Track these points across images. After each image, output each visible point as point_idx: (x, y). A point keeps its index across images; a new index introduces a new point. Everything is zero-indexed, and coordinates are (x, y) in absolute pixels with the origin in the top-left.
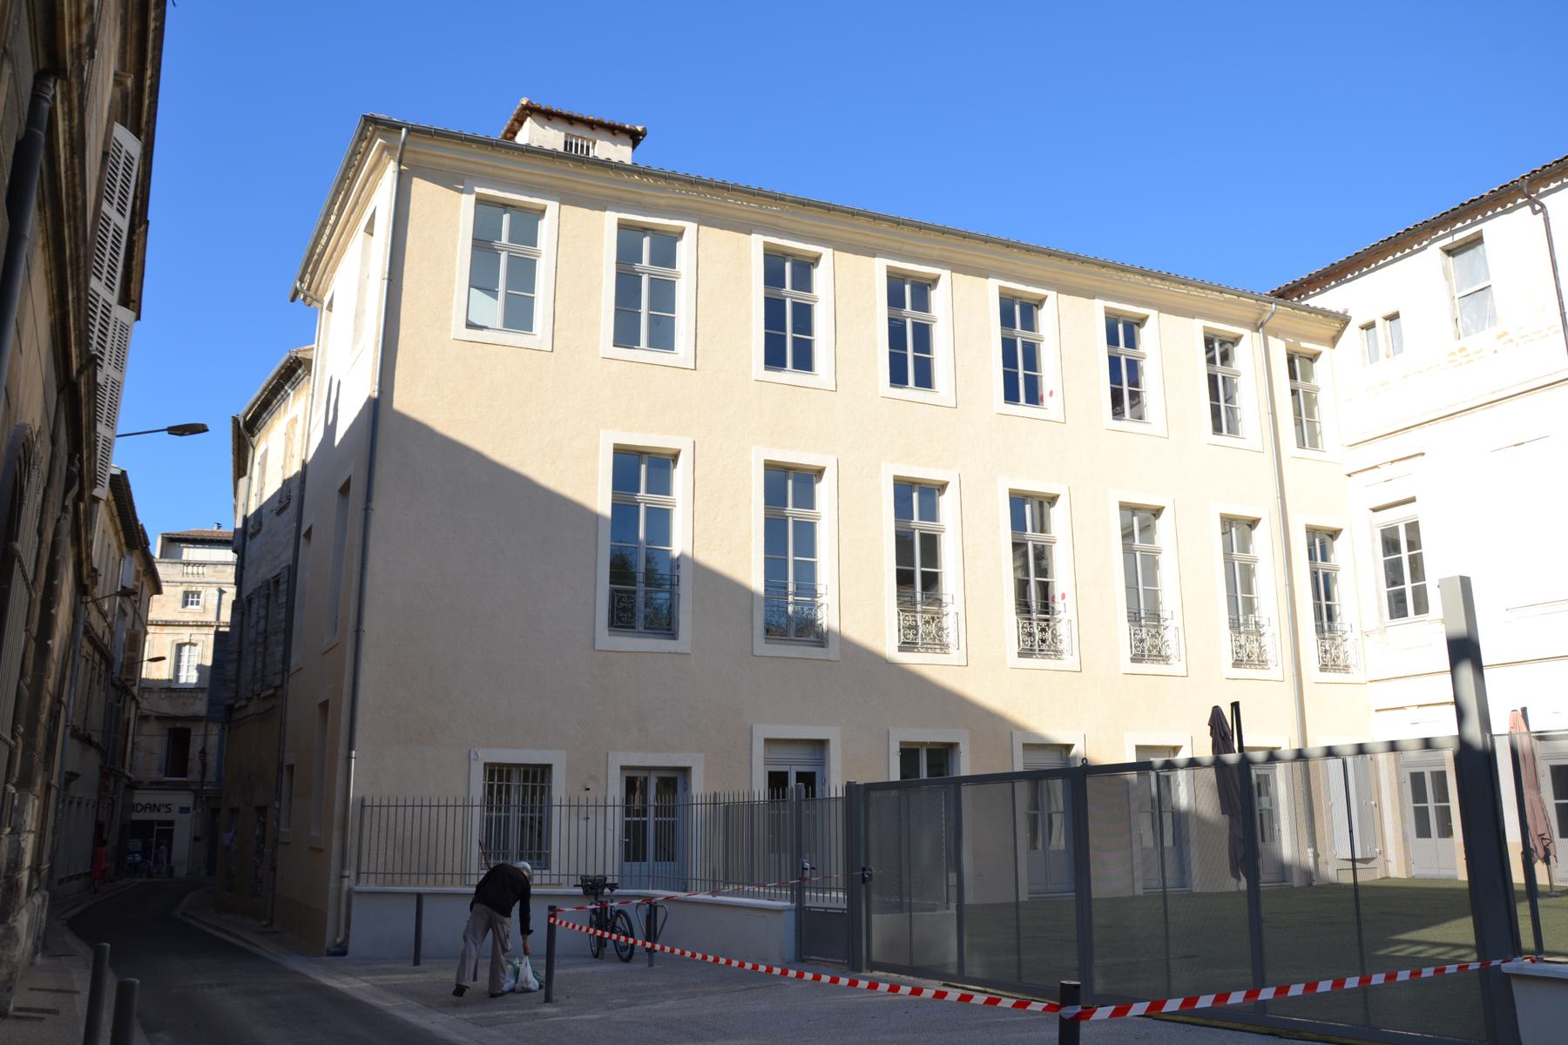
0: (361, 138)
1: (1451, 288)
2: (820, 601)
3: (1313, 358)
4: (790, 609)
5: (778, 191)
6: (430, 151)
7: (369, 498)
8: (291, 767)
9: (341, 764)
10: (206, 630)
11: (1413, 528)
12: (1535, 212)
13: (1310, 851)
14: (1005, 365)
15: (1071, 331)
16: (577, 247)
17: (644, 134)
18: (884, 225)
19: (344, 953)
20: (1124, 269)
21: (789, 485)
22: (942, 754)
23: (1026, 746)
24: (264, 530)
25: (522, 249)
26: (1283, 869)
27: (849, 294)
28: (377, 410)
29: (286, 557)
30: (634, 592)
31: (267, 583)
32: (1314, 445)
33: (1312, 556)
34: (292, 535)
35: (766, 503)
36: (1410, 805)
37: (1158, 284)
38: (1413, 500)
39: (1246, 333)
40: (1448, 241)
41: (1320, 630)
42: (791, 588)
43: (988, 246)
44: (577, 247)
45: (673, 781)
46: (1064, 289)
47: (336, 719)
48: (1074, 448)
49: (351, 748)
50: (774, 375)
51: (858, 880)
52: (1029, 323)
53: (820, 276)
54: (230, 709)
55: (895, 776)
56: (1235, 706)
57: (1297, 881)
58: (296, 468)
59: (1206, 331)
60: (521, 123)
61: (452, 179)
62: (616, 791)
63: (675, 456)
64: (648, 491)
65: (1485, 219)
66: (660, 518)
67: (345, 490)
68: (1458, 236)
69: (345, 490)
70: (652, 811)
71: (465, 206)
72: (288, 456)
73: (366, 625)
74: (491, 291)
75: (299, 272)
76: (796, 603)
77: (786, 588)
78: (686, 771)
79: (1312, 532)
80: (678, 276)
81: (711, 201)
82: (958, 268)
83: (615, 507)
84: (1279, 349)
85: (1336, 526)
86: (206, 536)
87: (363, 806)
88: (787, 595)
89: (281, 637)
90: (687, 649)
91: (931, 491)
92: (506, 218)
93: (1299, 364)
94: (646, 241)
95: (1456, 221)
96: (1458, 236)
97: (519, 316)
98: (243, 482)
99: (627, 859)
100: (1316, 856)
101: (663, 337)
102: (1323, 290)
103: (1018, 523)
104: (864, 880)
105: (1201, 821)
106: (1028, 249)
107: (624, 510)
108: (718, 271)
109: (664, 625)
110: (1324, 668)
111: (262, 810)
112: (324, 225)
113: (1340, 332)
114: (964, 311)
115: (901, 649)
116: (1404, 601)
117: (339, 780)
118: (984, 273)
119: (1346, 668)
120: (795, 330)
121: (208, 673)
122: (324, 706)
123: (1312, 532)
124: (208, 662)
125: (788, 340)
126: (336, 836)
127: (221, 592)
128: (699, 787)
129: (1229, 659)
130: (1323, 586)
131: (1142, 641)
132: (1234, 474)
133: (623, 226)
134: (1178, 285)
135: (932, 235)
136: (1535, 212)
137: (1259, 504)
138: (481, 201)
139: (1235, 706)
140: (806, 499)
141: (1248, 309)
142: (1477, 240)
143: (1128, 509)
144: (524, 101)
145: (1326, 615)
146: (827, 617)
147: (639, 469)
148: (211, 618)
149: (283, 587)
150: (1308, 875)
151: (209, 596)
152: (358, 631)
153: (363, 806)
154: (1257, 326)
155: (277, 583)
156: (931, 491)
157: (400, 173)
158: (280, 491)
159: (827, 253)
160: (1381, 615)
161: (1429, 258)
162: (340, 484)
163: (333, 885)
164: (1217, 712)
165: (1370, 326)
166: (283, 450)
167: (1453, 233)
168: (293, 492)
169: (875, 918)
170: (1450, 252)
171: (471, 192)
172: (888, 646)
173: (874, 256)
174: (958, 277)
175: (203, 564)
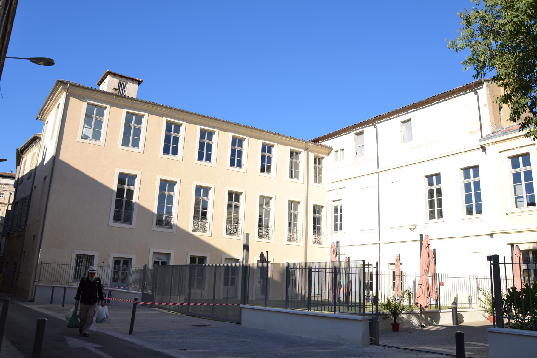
0: (56, 85)
2: (172, 217)
4: (164, 218)
6: (75, 90)
7: (50, 183)
8: (25, 252)
9: (37, 252)
10: (4, 205)
11: (341, 207)
12: (475, 94)
16: (114, 118)
17: (142, 81)
19: (33, 301)
21: (166, 186)
22: (202, 259)
24: (23, 183)
25: (99, 118)
26: (297, 295)
27: (189, 135)
28: (55, 159)
29: (29, 192)
30: (121, 212)
31: (23, 199)
32: (320, 182)
33: (315, 212)
34: (31, 186)
38: (341, 200)
39: (303, 151)
41: (314, 232)
44: (114, 118)
45: (127, 262)
46: (250, 136)
47: (37, 240)
48: (249, 181)
49: (40, 248)
51: (154, 287)
53: (182, 129)
54: (9, 234)
55: (188, 263)
56: (267, 252)
58: (34, 167)
59: (291, 149)
60: (107, 76)
61: (81, 98)
62: (111, 263)
64: (128, 185)
65: (365, 127)
66: (130, 193)
67: (45, 178)
68: (359, 131)
69: (45, 178)
70: (121, 269)
71: (84, 105)
72: (32, 163)
73: (47, 216)
74: (90, 126)
75: (39, 113)
78: (131, 259)
81: (153, 108)
82: (220, 129)
83: (118, 189)
84: (312, 156)
85: (323, 205)
86: (7, 175)
87: (42, 263)
89: (25, 215)
90: (134, 227)
91: (206, 190)
92: (95, 109)
93: (318, 160)
94: (134, 117)
96: (359, 131)
97: (97, 136)
98: (19, 167)
99: (114, 281)
101: (136, 144)
105: (274, 281)
107: (120, 191)
108: (153, 127)
109: (128, 220)
110: (314, 243)
111: (15, 263)
112: (46, 103)
117: (36, 256)
119: (321, 243)
120: (207, 151)
121: (4, 219)
122: (34, 236)
124: (4, 216)
125: (171, 146)
126: (34, 270)
127: (11, 194)
128: (134, 263)
129: (286, 239)
130: (317, 221)
132: (295, 190)
133: (127, 113)
134: (283, 138)
135: (214, 121)
136: (475, 94)
137: (300, 197)
138: (89, 104)
139: (267, 252)
141: (304, 145)
142: (362, 133)
143: (262, 197)
144: (108, 71)
145: (316, 229)
146: (174, 221)
147: (125, 179)
148: (7, 202)
149: (27, 201)
151: (7, 195)
152: (45, 217)
153: (42, 263)
154: (306, 149)
155: (26, 199)
156: (206, 190)
157: (67, 95)
158: (29, 173)
159: (184, 123)
161: (351, 136)
162: (44, 177)
163: (32, 283)
164: (262, 254)
165: (337, 151)
166: (31, 161)
168: (33, 174)
169: (157, 296)
171: (86, 102)
172: (190, 229)
174: (221, 132)
175: (5, 184)
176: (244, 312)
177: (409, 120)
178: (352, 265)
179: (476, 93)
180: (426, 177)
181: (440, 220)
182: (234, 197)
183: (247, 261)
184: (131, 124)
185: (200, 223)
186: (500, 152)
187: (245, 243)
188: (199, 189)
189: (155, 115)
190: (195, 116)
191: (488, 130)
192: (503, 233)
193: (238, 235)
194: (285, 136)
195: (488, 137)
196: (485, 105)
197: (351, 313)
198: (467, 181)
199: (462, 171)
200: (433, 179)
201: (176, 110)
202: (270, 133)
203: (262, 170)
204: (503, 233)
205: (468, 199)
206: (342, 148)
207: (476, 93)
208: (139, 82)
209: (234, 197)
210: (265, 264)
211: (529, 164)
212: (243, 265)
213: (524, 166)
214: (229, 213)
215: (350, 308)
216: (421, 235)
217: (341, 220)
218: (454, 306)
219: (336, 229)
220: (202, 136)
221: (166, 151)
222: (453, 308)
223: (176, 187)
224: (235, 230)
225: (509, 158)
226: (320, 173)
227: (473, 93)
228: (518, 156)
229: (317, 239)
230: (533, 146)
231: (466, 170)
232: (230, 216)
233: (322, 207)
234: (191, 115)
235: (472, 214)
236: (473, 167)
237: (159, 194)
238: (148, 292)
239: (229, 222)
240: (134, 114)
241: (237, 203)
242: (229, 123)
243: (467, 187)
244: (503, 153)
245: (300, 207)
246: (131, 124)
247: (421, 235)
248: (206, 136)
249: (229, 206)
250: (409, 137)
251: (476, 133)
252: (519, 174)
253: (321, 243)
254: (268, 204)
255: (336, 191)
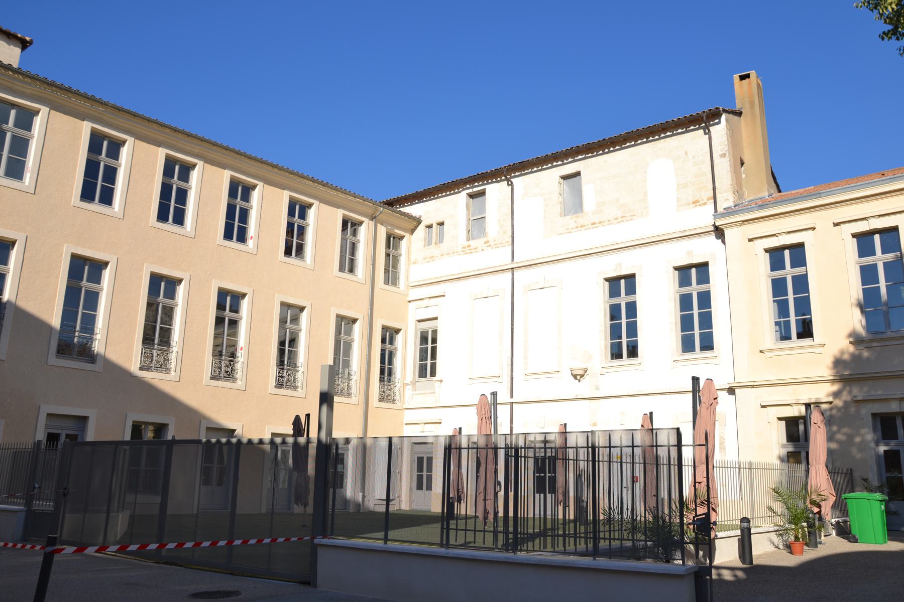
1: (469, 214)
3: (401, 238)
4: (76, 339)
5: (104, 100)
11: (435, 332)
13: (361, 494)
14: (227, 218)
15: (268, 206)
17: (31, 43)
18: (167, 130)
20: (302, 177)
21: (85, 270)
23: (208, 429)
26: (346, 502)
27: (139, 165)
33: (383, 341)
35: (149, 294)
36: (415, 473)
37: (321, 187)
38: (436, 318)
40: (470, 191)
41: (382, 379)
42: (78, 328)
43: (227, 152)
46: (268, 182)
48: (260, 270)
50: (161, 225)
52: (303, 216)
53: (194, 175)
55: (128, 437)
57: (351, 509)
59: (344, 216)
63: (13, 243)
64: (88, 281)
68: (475, 189)
76: (79, 337)
77: (75, 327)
79: (385, 329)
80: (32, 137)
82: (207, 161)
84: (382, 231)
85: (399, 327)
88: (75, 331)
93: (393, 240)
94: (13, 113)
95: (474, 181)
96: (475, 189)
100: (364, 497)
102: (412, 204)
103: (221, 306)
104: (65, 495)
106: (250, 158)
110: (381, 400)
113: (416, 227)
114: (207, 186)
115: (141, 369)
116: (426, 369)
118: (224, 166)
119: (394, 401)
120: (176, 202)
123: (385, 329)
125: (98, 185)
130: (387, 358)
131: (282, 377)
132: (348, 294)
134: (332, 190)
135: (195, 141)
140: (171, 294)
141: (369, 208)
143: (285, 306)
145: (386, 373)
146: (98, 347)
150: (358, 506)
154: (372, 218)
160: (414, 375)
161: (460, 199)
164: (297, 418)
165: (430, 227)
167: (473, 187)
169: (67, 515)
170: (471, 196)
173: (159, 146)
174: (208, 166)
176: (322, 554)
177: (578, 174)
178: (571, 442)
179: (708, 132)
180: (676, 269)
181: (633, 361)
182: (228, 302)
183: (329, 432)
184: (4, 126)
185: (155, 353)
186: (750, 240)
187: (325, 388)
188: (156, 280)
189: (66, 113)
190: (155, 126)
191: (726, 200)
192: (753, 386)
193: (234, 380)
194: (336, 189)
195: (728, 212)
196: (723, 155)
197: (576, 553)
198: (615, 301)
199: (677, 272)
200: (622, 285)
201: (115, 108)
202: (307, 178)
203: (288, 252)
204: (753, 386)
205: (615, 332)
206: (440, 220)
207: (708, 132)
208: (24, 44)
209: (228, 302)
210: (302, 440)
211: (707, 281)
212: (319, 441)
213: (698, 283)
214: (218, 336)
215: (561, 539)
216: (695, 380)
217: (434, 356)
218: (745, 525)
219: (422, 373)
220: (168, 171)
221: (87, 194)
222: (742, 530)
223: (107, 274)
224: (229, 369)
225: (766, 251)
226: (395, 266)
227: (701, 131)
228: (872, 233)
229: (387, 392)
230: (810, 232)
231: (613, 282)
232: (219, 341)
233: (397, 331)
234: (146, 123)
235: (621, 357)
236: (626, 277)
237: (68, 287)
238: (45, 505)
239: (217, 353)
240: (14, 105)
241: (233, 315)
242: (227, 149)
243: (615, 312)
244: (756, 241)
245: (357, 327)
246: (4, 126)
247: (695, 380)
248: (176, 173)
249: (219, 321)
250: (575, 205)
251: (705, 204)
252: (783, 280)
253: (394, 401)
254: (295, 320)
255: (426, 302)
